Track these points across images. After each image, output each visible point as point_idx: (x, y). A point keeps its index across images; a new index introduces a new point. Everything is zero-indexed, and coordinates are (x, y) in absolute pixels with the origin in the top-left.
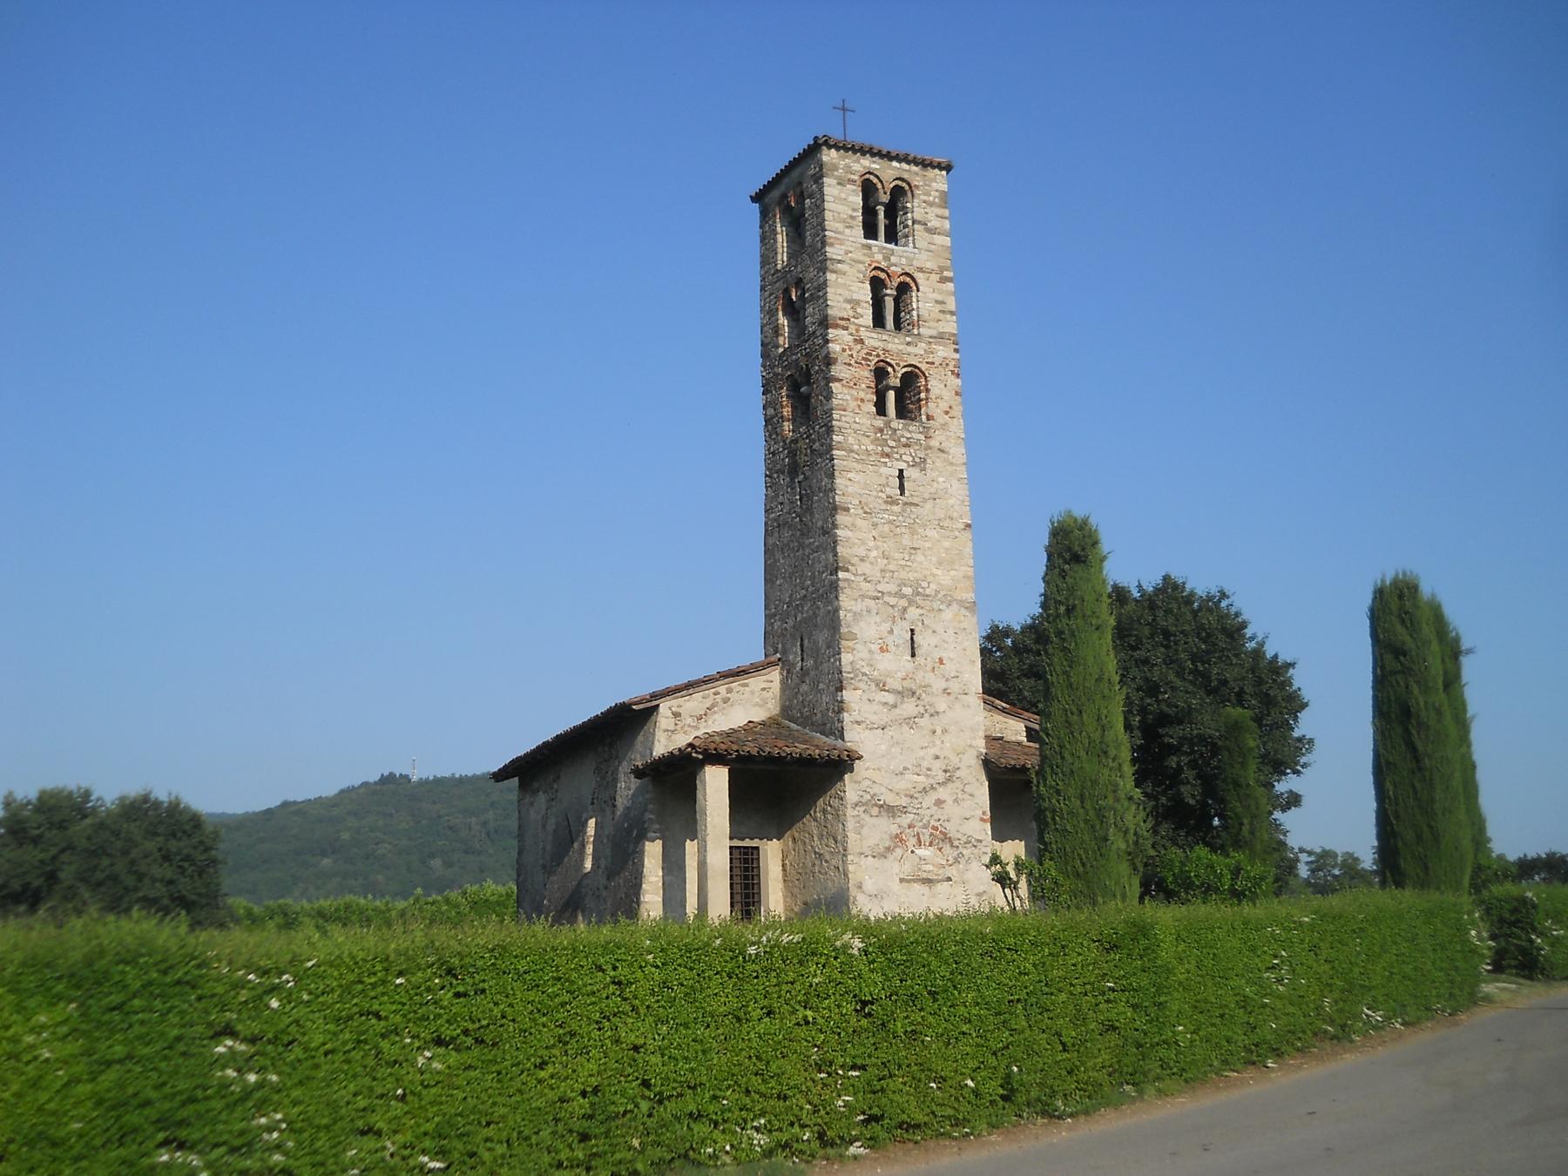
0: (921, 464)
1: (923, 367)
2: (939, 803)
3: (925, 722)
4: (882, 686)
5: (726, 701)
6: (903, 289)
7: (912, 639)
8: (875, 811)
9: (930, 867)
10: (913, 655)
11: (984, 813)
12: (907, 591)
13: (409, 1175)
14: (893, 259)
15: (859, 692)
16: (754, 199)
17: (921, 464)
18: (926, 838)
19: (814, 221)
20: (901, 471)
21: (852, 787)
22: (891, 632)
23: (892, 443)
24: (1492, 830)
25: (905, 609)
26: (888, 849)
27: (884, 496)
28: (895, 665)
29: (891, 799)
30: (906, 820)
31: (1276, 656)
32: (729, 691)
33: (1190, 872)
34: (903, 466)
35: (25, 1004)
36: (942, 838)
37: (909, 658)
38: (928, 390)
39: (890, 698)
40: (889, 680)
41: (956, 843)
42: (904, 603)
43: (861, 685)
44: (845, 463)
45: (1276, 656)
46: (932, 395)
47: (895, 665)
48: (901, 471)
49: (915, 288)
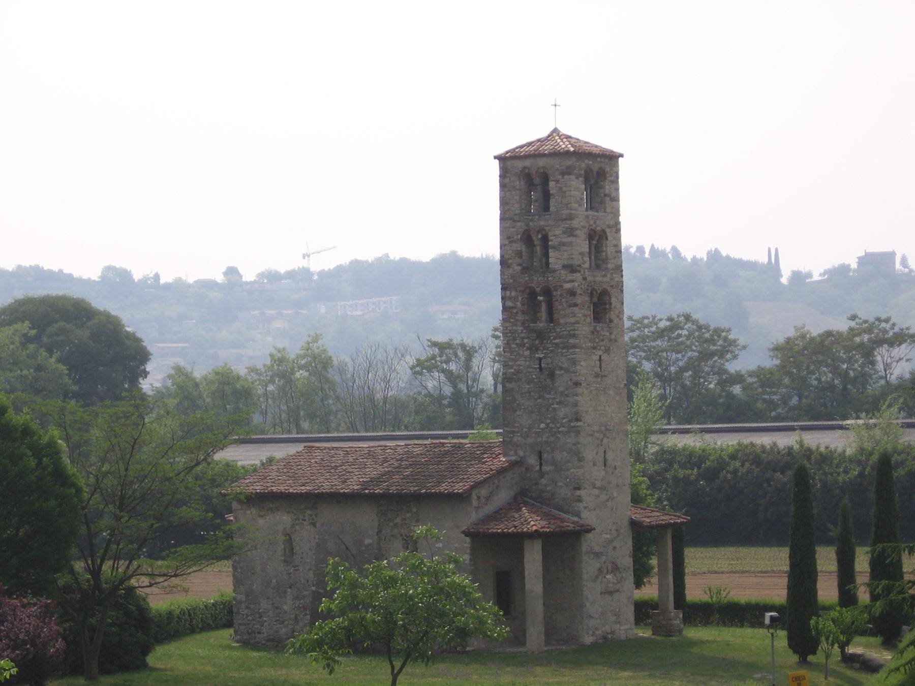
0: (607, 351)
1: (609, 289)
2: (615, 548)
3: (609, 504)
4: (594, 487)
5: (498, 487)
6: (600, 237)
7: (605, 456)
8: (592, 556)
9: (611, 585)
10: (605, 465)
11: (630, 552)
12: (603, 428)
13: (796, 683)
14: (598, 222)
15: (586, 490)
16: (500, 158)
17: (607, 351)
18: (610, 568)
19: (614, 239)
20: (600, 356)
21: (590, 542)
22: (597, 453)
23: (597, 340)
24: (687, 592)
25: (602, 440)
26: (597, 577)
27: (593, 373)
28: (598, 473)
29: (597, 549)
30: (604, 558)
31: (299, 267)
32: (499, 481)
33: (407, 592)
34: (601, 353)
35: (615, 617)
36: (615, 569)
37: (603, 468)
38: (610, 304)
39: (596, 492)
40: (596, 482)
41: (621, 570)
42: (602, 436)
43: (587, 486)
44: (580, 356)
45: (299, 267)
46: (613, 306)
47: (598, 473)
48: (600, 356)
49: (604, 238)
